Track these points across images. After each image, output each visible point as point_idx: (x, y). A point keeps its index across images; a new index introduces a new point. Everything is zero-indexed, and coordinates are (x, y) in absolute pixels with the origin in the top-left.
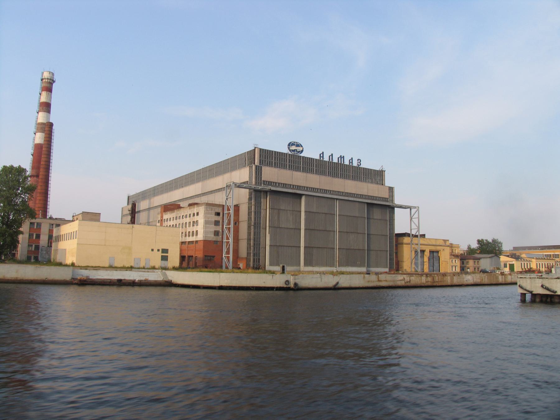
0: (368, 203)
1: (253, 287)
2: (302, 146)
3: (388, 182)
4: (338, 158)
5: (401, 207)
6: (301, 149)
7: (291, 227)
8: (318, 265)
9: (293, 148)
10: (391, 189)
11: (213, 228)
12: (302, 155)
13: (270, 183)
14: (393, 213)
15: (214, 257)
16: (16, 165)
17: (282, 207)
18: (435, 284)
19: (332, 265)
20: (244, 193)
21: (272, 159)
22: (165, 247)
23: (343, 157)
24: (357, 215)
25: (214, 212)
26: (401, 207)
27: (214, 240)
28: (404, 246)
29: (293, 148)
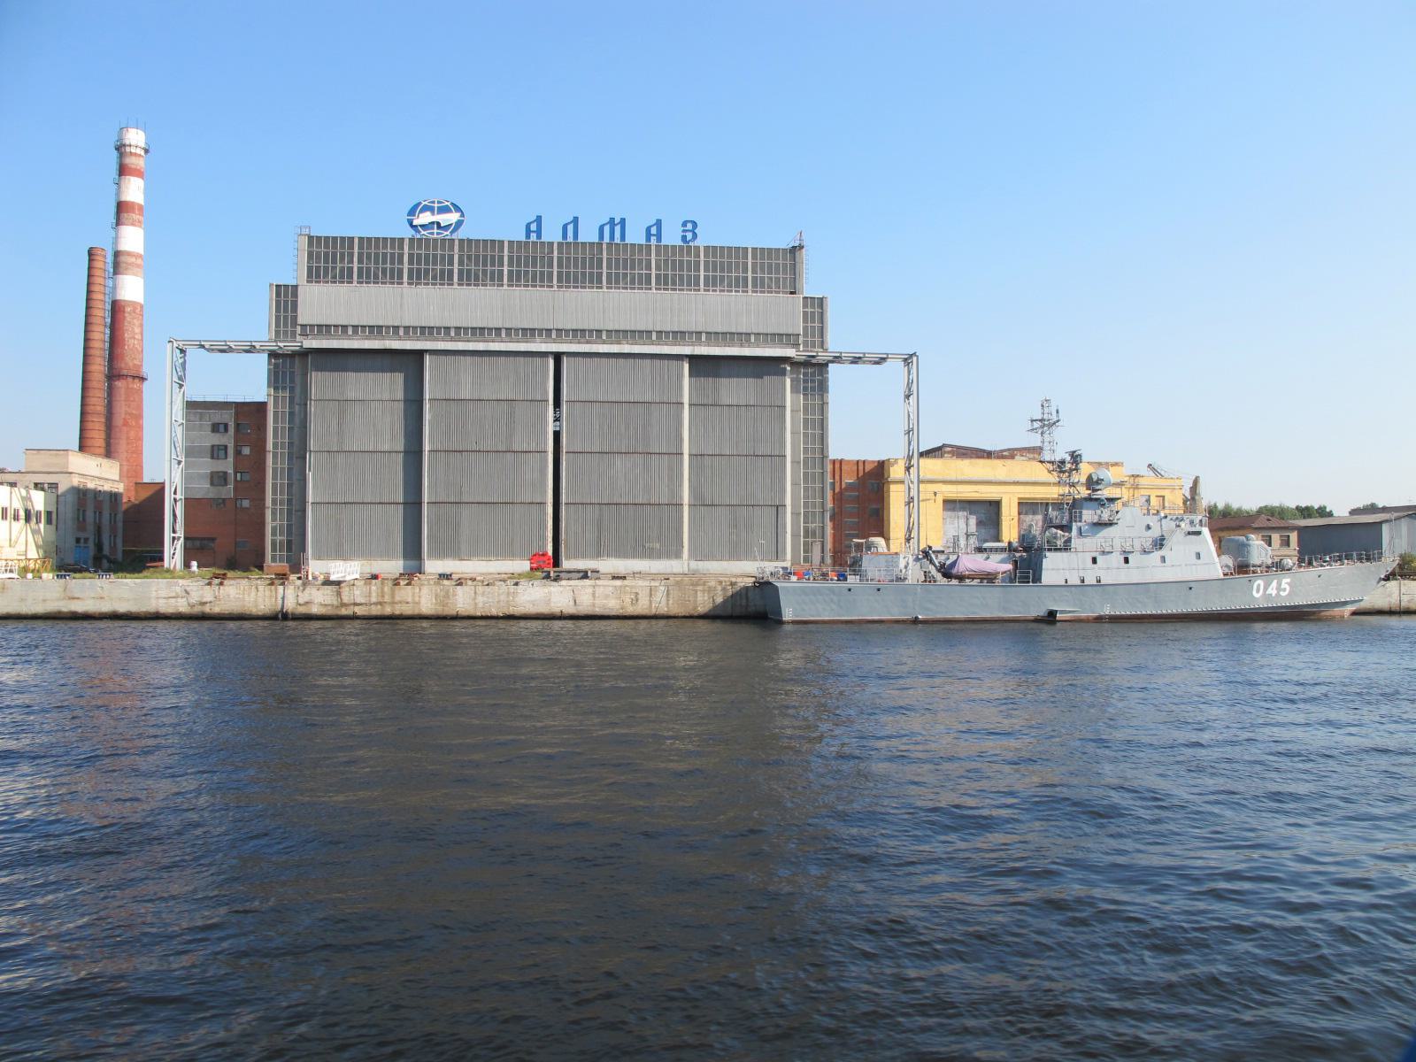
0: (692, 359)
1: (101, 614)
2: (458, 209)
3: (811, 286)
4: (601, 229)
5: (837, 359)
6: (453, 217)
7: (386, 447)
8: (475, 552)
9: (425, 218)
10: (817, 307)
11: (207, 466)
12: (462, 234)
13: (324, 329)
14: (823, 388)
15: (213, 540)
16: (1276, 504)
17: (351, 395)
18: (344, 612)
19: (124, 542)
20: (259, 366)
21: (351, 261)
22: (1194, 556)
23: (623, 221)
24: (648, 398)
25: (207, 424)
26: (837, 359)
27: (211, 496)
28: (402, 449)
29: (425, 218)
